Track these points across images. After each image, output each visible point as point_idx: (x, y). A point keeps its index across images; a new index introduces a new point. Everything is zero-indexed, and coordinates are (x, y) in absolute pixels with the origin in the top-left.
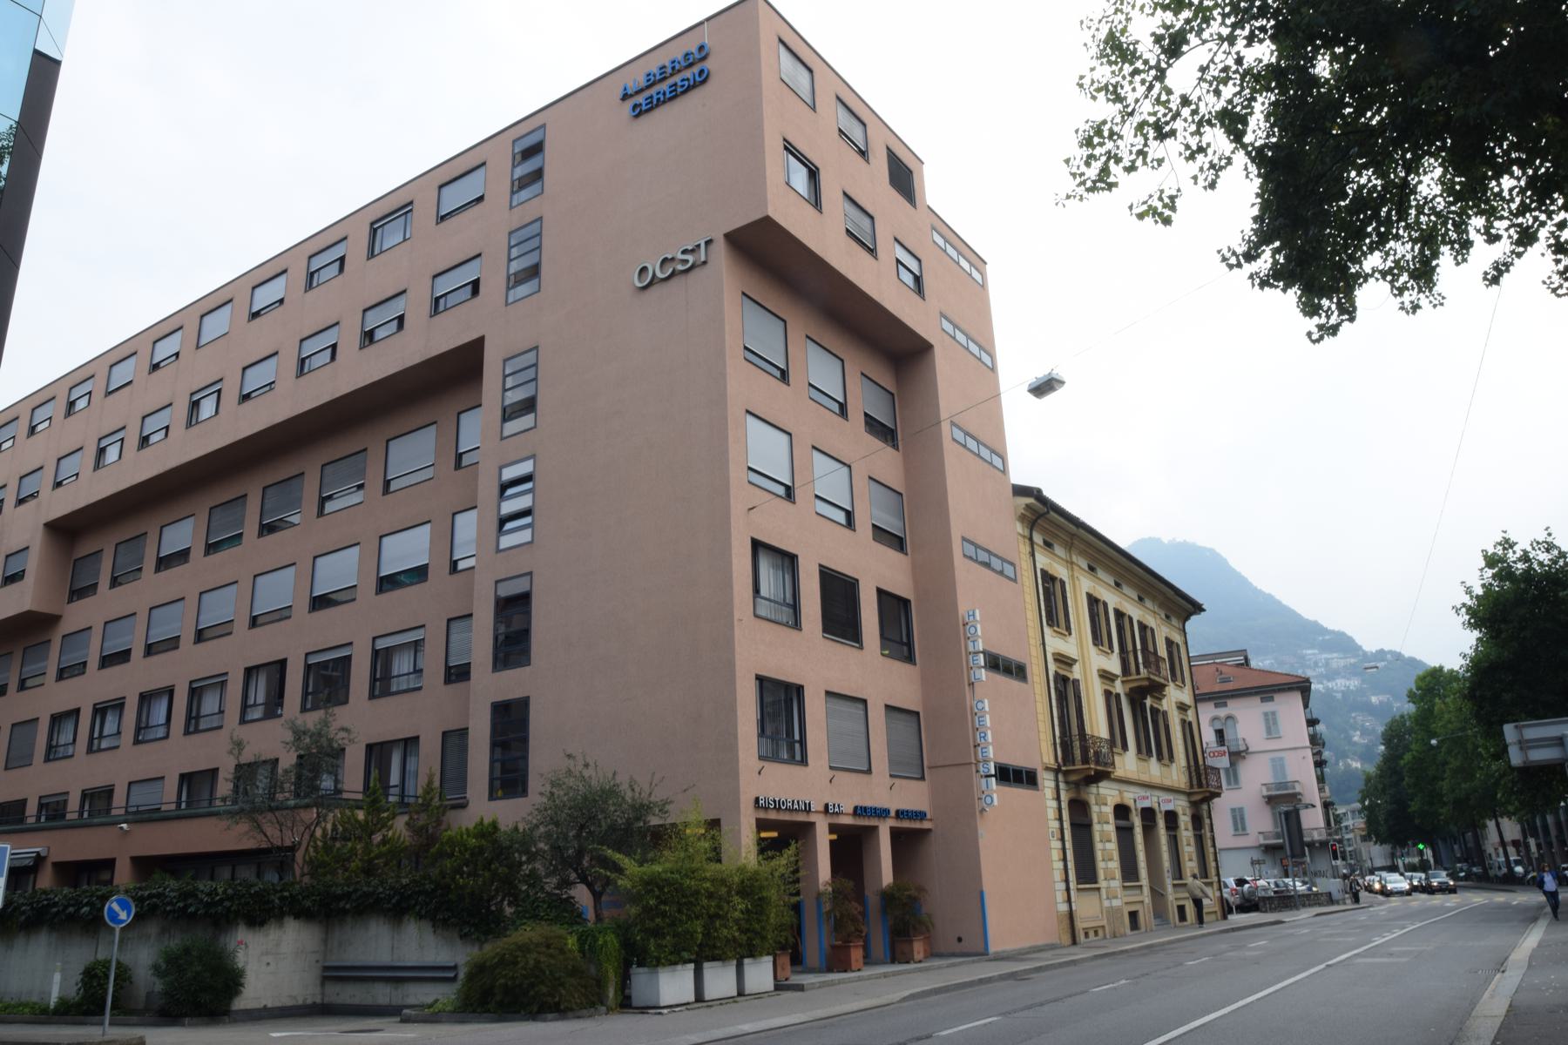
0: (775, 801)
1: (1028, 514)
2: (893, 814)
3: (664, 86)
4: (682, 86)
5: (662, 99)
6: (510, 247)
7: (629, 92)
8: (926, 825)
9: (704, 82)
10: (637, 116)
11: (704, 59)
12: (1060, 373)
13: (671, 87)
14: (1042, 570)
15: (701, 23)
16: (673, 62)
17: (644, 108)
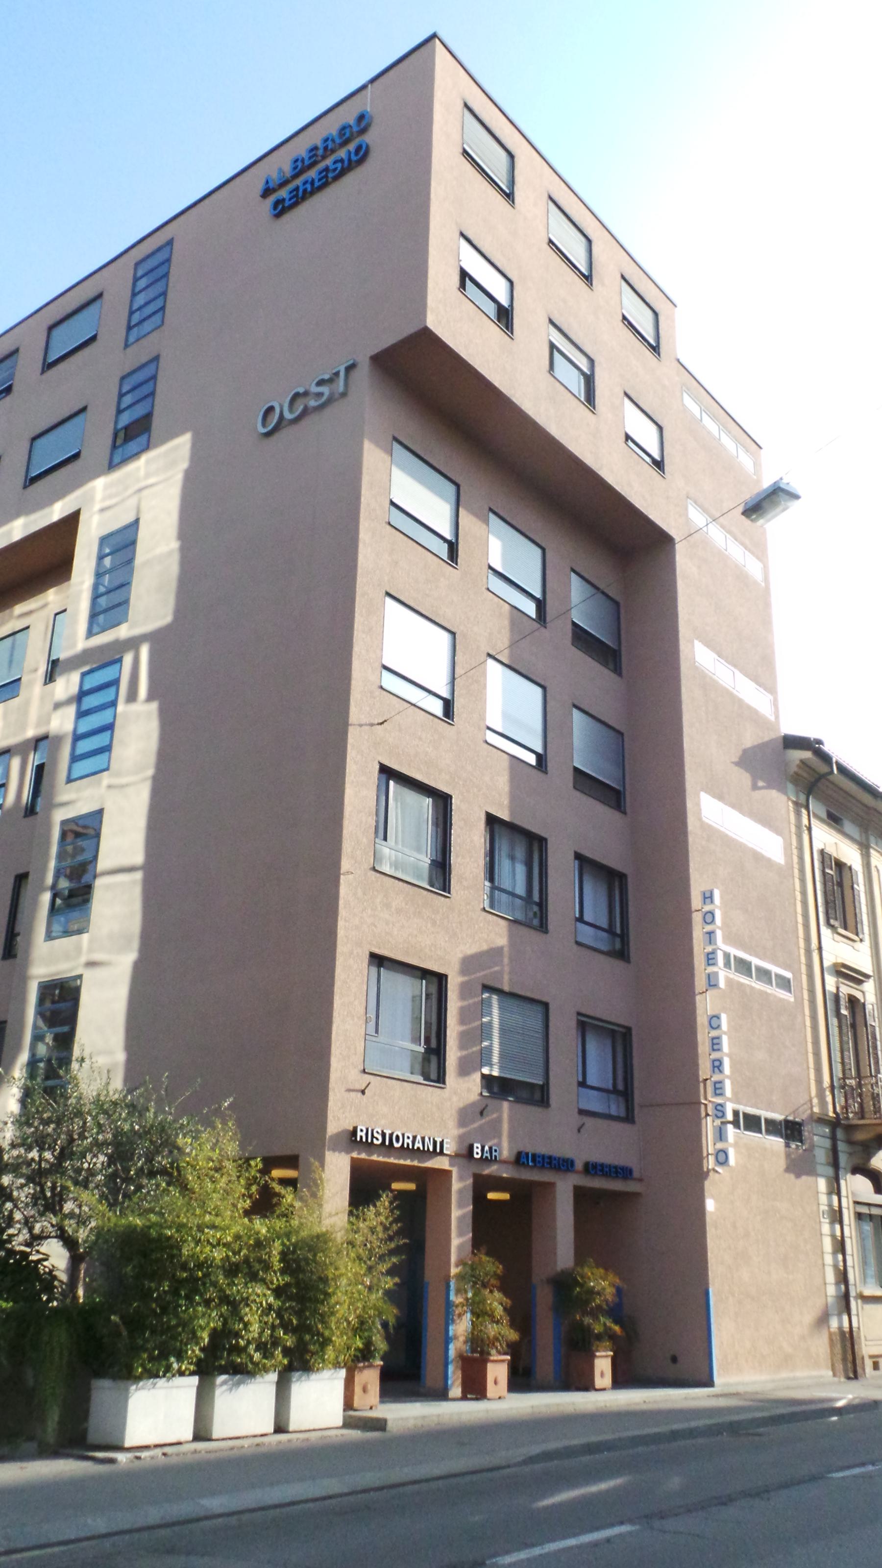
0: (383, 1135)
1: (805, 775)
2: (579, 1165)
3: (313, 174)
4: (335, 169)
5: (309, 189)
6: (121, 395)
7: (271, 185)
8: (631, 1187)
9: (361, 161)
10: (278, 216)
11: (363, 131)
12: (793, 483)
13: (320, 173)
14: (822, 852)
15: (364, 87)
16: (326, 140)
17: (287, 203)
